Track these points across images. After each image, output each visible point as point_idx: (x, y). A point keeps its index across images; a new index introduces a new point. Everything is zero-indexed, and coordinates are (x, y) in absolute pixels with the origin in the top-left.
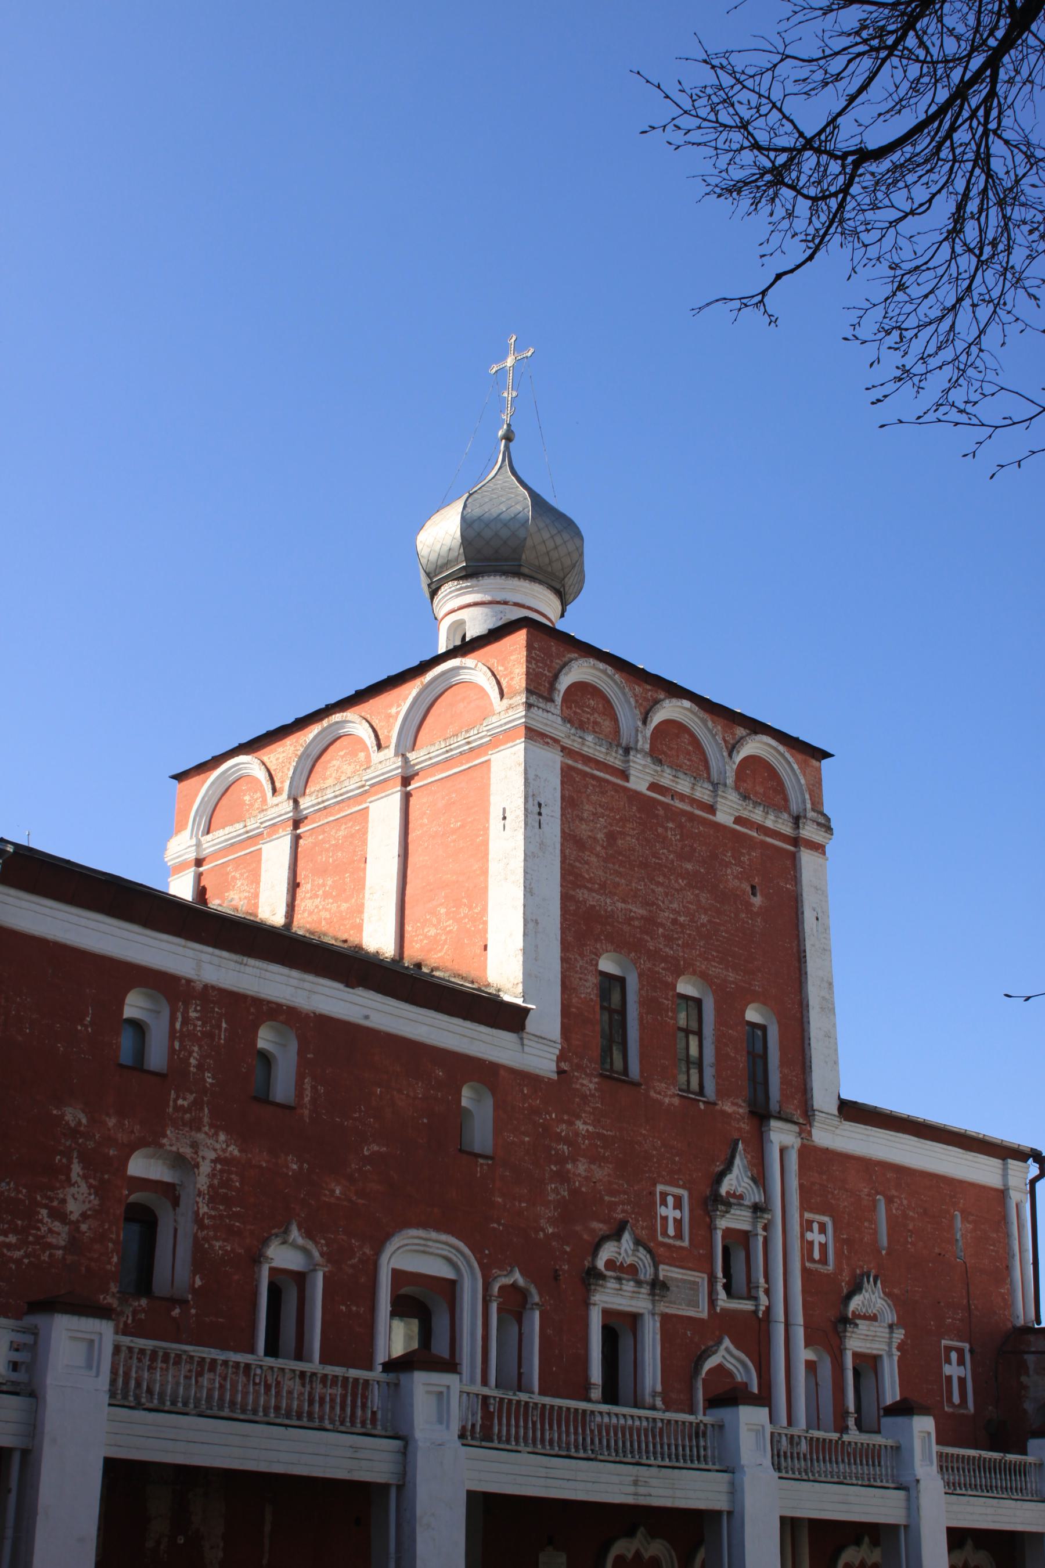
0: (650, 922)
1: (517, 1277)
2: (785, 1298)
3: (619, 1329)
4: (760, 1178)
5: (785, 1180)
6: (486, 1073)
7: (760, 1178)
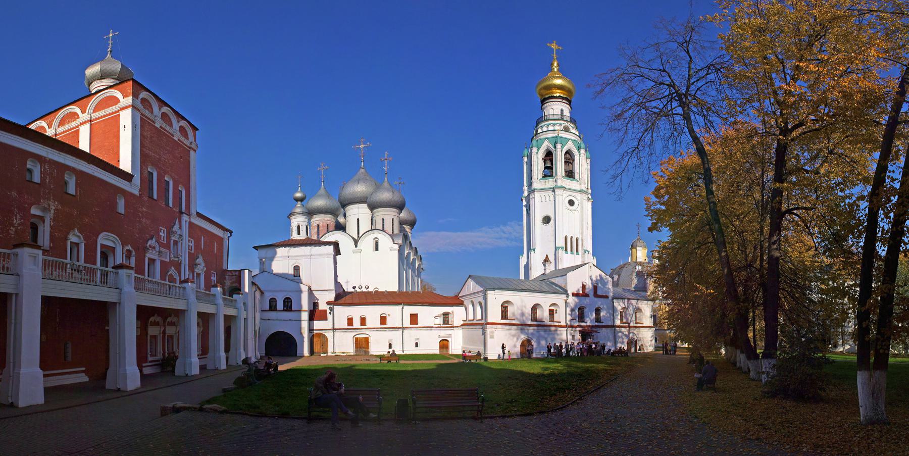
3: (152, 261)
4: (180, 228)
5: (186, 227)
7: (180, 228)
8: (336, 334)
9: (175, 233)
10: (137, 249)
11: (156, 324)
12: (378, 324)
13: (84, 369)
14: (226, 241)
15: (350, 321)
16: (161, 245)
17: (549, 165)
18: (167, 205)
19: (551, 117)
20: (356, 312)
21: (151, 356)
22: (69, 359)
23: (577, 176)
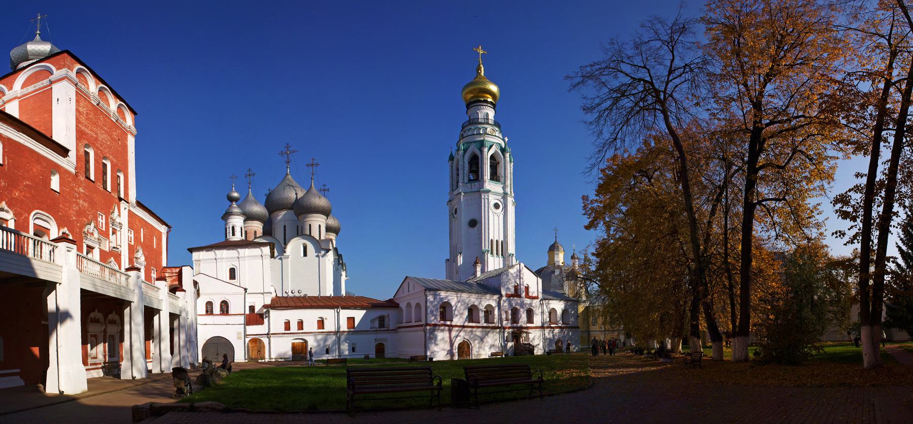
0: (96, 139)
5: (124, 219)
7: (119, 215)
8: (272, 339)
13: (18, 371)
15: (287, 325)
16: (101, 232)
17: (474, 169)
18: (105, 188)
20: (293, 315)
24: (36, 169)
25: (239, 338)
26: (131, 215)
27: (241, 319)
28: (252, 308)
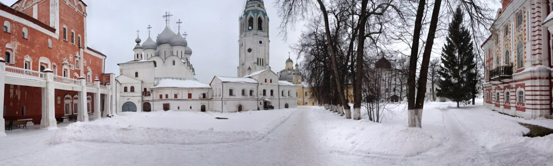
0: (69, 22)
1: (55, 64)
2: (82, 69)
4: (79, 55)
5: (82, 56)
6: (51, 37)
7: (79, 55)
9: (76, 57)
10: (58, 64)
11: (68, 98)
12: (173, 97)
14: (103, 61)
19: (288, 116)
21: (66, 113)
22: (25, 114)
23: (263, 29)
24: (43, 39)
25: (139, 102)
26: (85, 53)
27: (140, 94)
28: (145, 89)
